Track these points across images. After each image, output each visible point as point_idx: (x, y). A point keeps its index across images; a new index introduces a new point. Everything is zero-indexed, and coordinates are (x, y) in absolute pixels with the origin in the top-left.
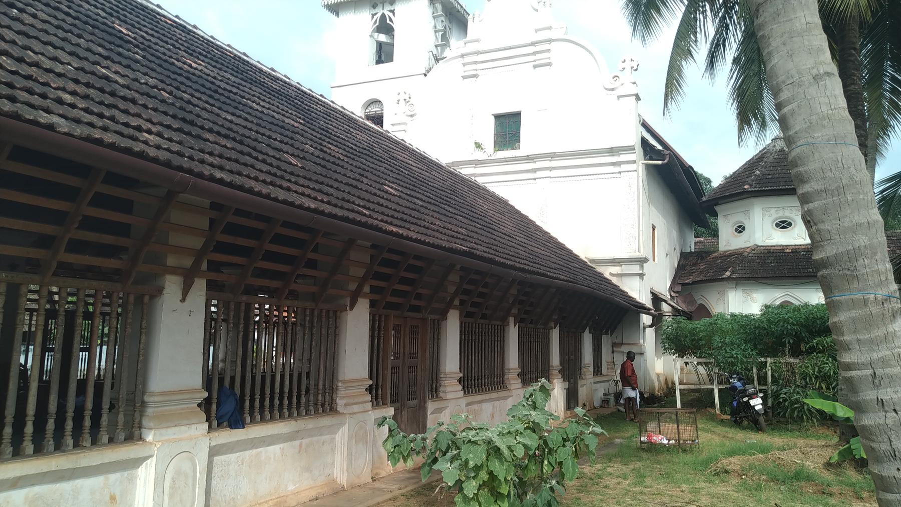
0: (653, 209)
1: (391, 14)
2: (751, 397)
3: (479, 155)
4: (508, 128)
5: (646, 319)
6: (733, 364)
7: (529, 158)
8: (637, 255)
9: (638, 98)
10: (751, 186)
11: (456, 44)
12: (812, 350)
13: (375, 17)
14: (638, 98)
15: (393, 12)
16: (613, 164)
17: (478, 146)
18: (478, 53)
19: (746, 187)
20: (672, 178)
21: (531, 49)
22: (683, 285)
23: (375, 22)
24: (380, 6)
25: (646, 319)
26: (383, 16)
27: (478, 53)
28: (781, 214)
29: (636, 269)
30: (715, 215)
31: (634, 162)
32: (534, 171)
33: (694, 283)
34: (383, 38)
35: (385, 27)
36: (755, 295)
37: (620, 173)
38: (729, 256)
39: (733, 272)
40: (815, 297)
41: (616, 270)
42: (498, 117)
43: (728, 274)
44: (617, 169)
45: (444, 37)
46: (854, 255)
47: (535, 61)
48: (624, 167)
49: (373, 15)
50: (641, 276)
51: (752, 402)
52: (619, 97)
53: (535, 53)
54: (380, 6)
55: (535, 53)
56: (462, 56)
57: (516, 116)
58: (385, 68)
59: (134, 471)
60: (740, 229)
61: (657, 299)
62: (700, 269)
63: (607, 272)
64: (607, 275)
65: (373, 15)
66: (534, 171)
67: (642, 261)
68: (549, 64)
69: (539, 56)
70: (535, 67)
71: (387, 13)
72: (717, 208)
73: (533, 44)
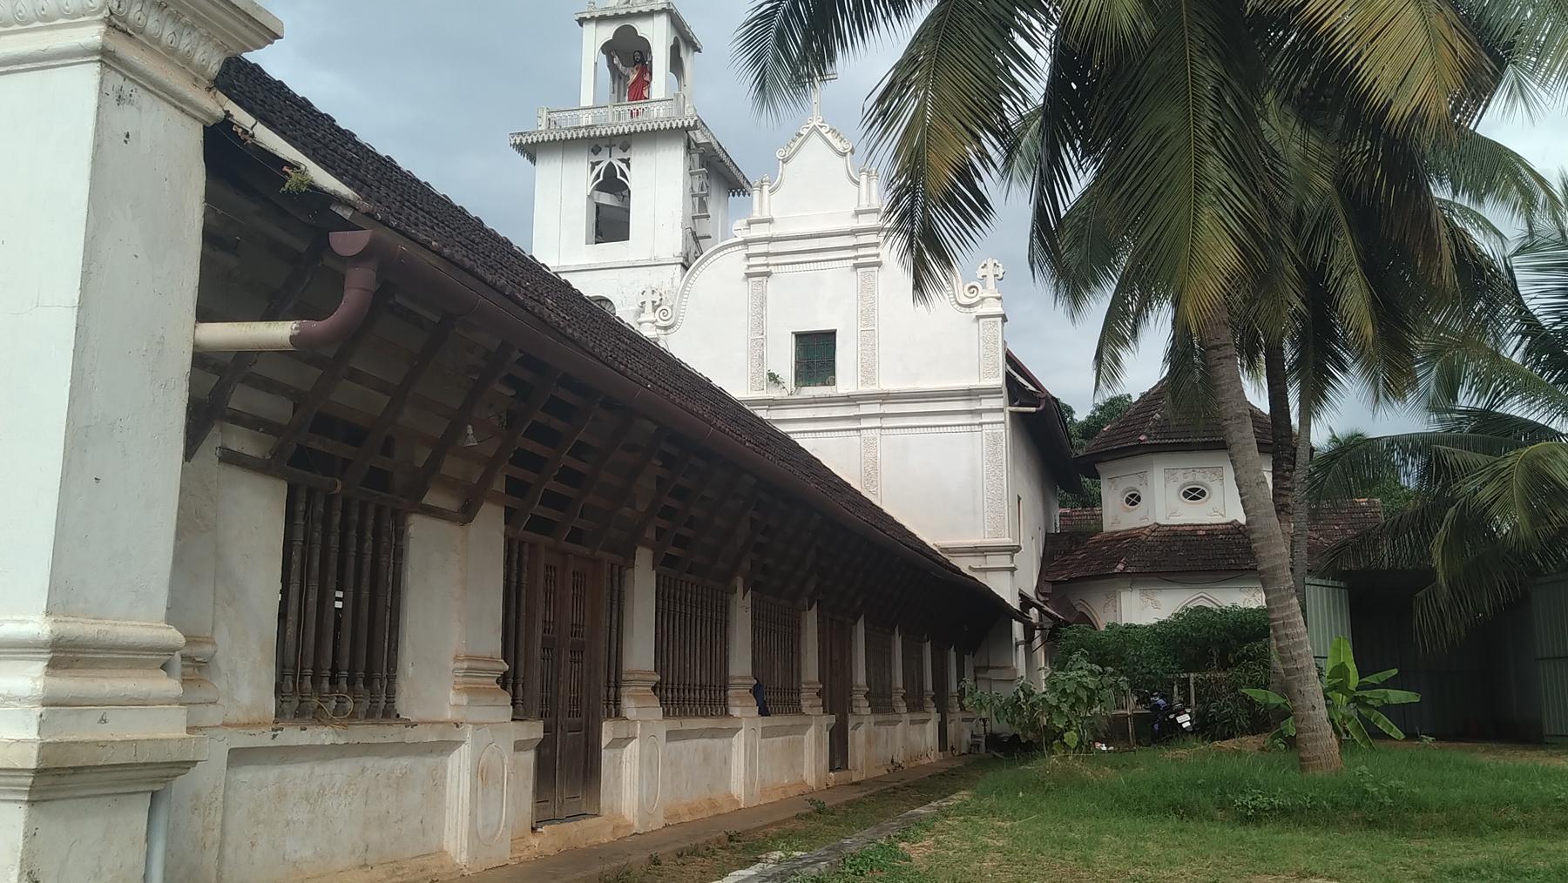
1: (623, 166)
3: (775, 394)
4: (816, 354)
5: (1018, 628)
6: (1151, 681)
7: (850, 400)
8: (1007, 540)
9: (1004, 319)
10: (1149, 436)
11: (731, 221)
12: (1239, 660)
13: (597, 168)
14: (1004, 319)
15: (627, 162)
16: (971, 412)
17: (773, 378)
19: (1142, 438)
22: (1054, 583)
23: (598, 176)
25: (1018, 628)
26: (611, 166)
27: (770, 240)
28: (1190, 479)
29: (1004, 561)
32: (858, 418)
34: (606, 199)
35: (612, 183)
38: (1119, 539)
40: (1249, 599)
41: (977, 562)
42: (800, 337)
43: (1120, 567)
44: (977, 421)
45: (703, 205)
47: (856, 258)
49: (594, 165)
50: (1012, 570)
51: (1179, 719)
52: (978, 318)
53: (855, 247)
55: (855, 247)
56: (746, 243)
57: (829, 337)
58: (612, 251)
60: (1133, 500)
61: (1026, 602)
62: (1079, 558)
63: (964, 564)
64: (965, 570)
65: (594, 165)
66: (858, 418)
68: (879, 264)
69: (862, 252)
70: (856, 266)
71: (616, 163)
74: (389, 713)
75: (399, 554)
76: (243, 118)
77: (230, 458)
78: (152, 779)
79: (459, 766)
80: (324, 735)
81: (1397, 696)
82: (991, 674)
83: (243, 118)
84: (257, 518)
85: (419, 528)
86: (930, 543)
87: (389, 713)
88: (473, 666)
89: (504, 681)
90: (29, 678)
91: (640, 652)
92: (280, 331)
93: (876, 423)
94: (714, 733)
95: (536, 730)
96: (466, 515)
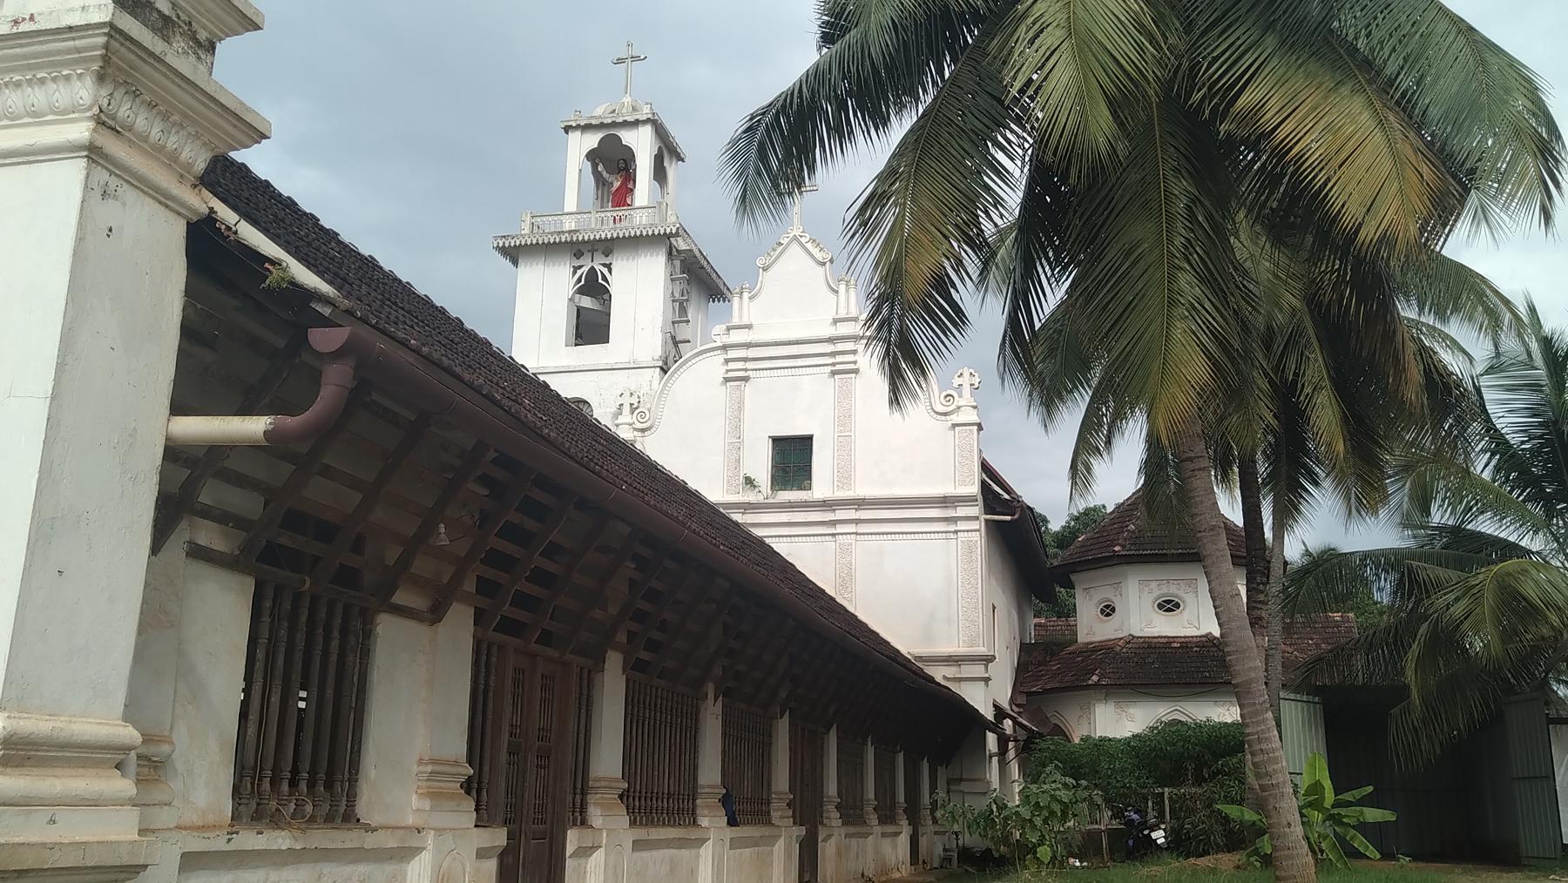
0: (994, 582)
1: (605, 271)
2: (1153, 828)
3: (751, 497)
4: (792, 458)
6: (1125, 796)
8: (982, 650)
10: (1123, 547)
14: (980, 428)
15: (609, 266)
17: (749, 482)
18: (748, 345)
19: (1117, 548)
20: (1012, 530)
21: (829, 348)
22: (1029, 694)
23: (579, 280)
24: (588, 256)
27: (748, 345)
28: (1165, 590)
29: (978, 670)
30: (1070, 586)
31: (977, 518)
32: (834, 523)
33: (1046, 691)
34: (587, 302)
35: (594, 287)
36: (1131, 711)
37: (956, 532)
39: (1101, 677)
40: (1225, 713)
41: (951, 671)
42: (777, 441)
43: (1095, 678)
44: (952, 528)
45: (683, 310)
46: (1250, 682)
47: (833, 364)
48: (961, 526)
51: (1154, 835)
52: (954, 426)
53: (833, 354)
54: (588, 256)
55: (833, 354)
57: (805, 442)
59: (582, 861)
60: (1108, 611)
61: (1000, 713)
62: (1055, 668)
63: (939, 673)
64: (939, 679)
66: (834, 523)
67: (987, 660)
68: (856, 371)
69: (839, 359)
70: (834, 373)
72: (1073, 577)
73: (831, 340)
74: (349, 818)
75: (366, 653)
76: (226, 214)
77: (197, 553)
80: (281, 840)
82: (964, 786)
83: (226, 214)
84: (222, 615)
85: (388, 628)
86: (904, 651)
87: (349, 818)
88: (437, 768)
89: (467, 786)
91: (607, 759)
92: (255, 426)
94: (682, 843)
96: (435, 614)
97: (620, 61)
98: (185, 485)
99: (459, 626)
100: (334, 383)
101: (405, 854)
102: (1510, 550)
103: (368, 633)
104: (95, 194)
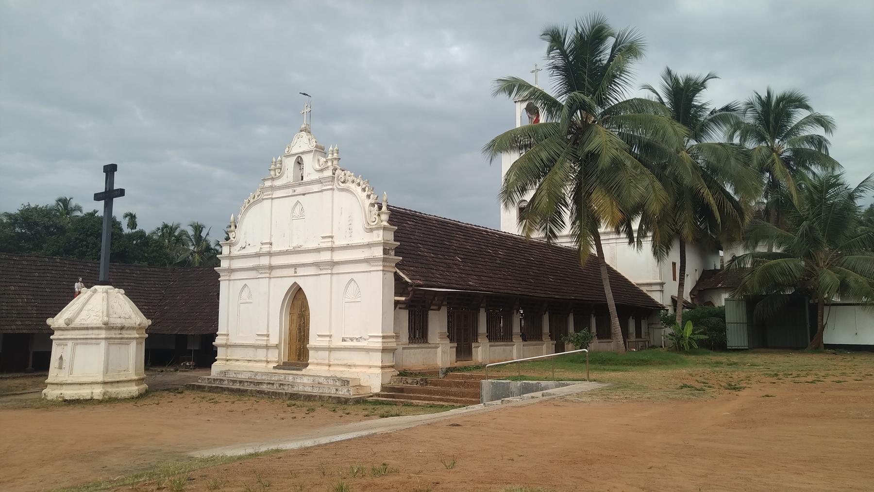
8: (659, 281)
41: (649, 288)
63: (644, 289)
74: (427, 342)
75: (427, 318)
76: (398, 271)
77: (400, 308)
78: (393, 351)
79: (439, 350)
80: (416, 346)
81: (702, 337)
82: (653, 326)
83: (398, 271)
84: (405, 315)
85: (430, 312)
86: (633, 282)
87: (427, 342)
88: (441, 334)
89: (448, 336)
90: (380, 340)
91: (483, 328)
92: (403, 299)
93: (614, 241)
94: (539, 345)
95: (456, 345)
96: (439, 309)
97: (533, 72)
98: (397, 303)
99: (444, 311)
100: (411, 294)
101: (437, 348)
102: (779, 264)
103: (427, 315)
104: (384, 274)
